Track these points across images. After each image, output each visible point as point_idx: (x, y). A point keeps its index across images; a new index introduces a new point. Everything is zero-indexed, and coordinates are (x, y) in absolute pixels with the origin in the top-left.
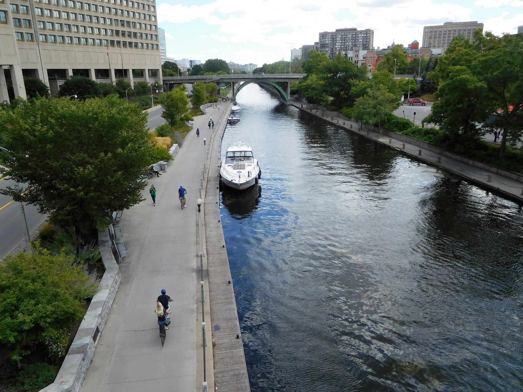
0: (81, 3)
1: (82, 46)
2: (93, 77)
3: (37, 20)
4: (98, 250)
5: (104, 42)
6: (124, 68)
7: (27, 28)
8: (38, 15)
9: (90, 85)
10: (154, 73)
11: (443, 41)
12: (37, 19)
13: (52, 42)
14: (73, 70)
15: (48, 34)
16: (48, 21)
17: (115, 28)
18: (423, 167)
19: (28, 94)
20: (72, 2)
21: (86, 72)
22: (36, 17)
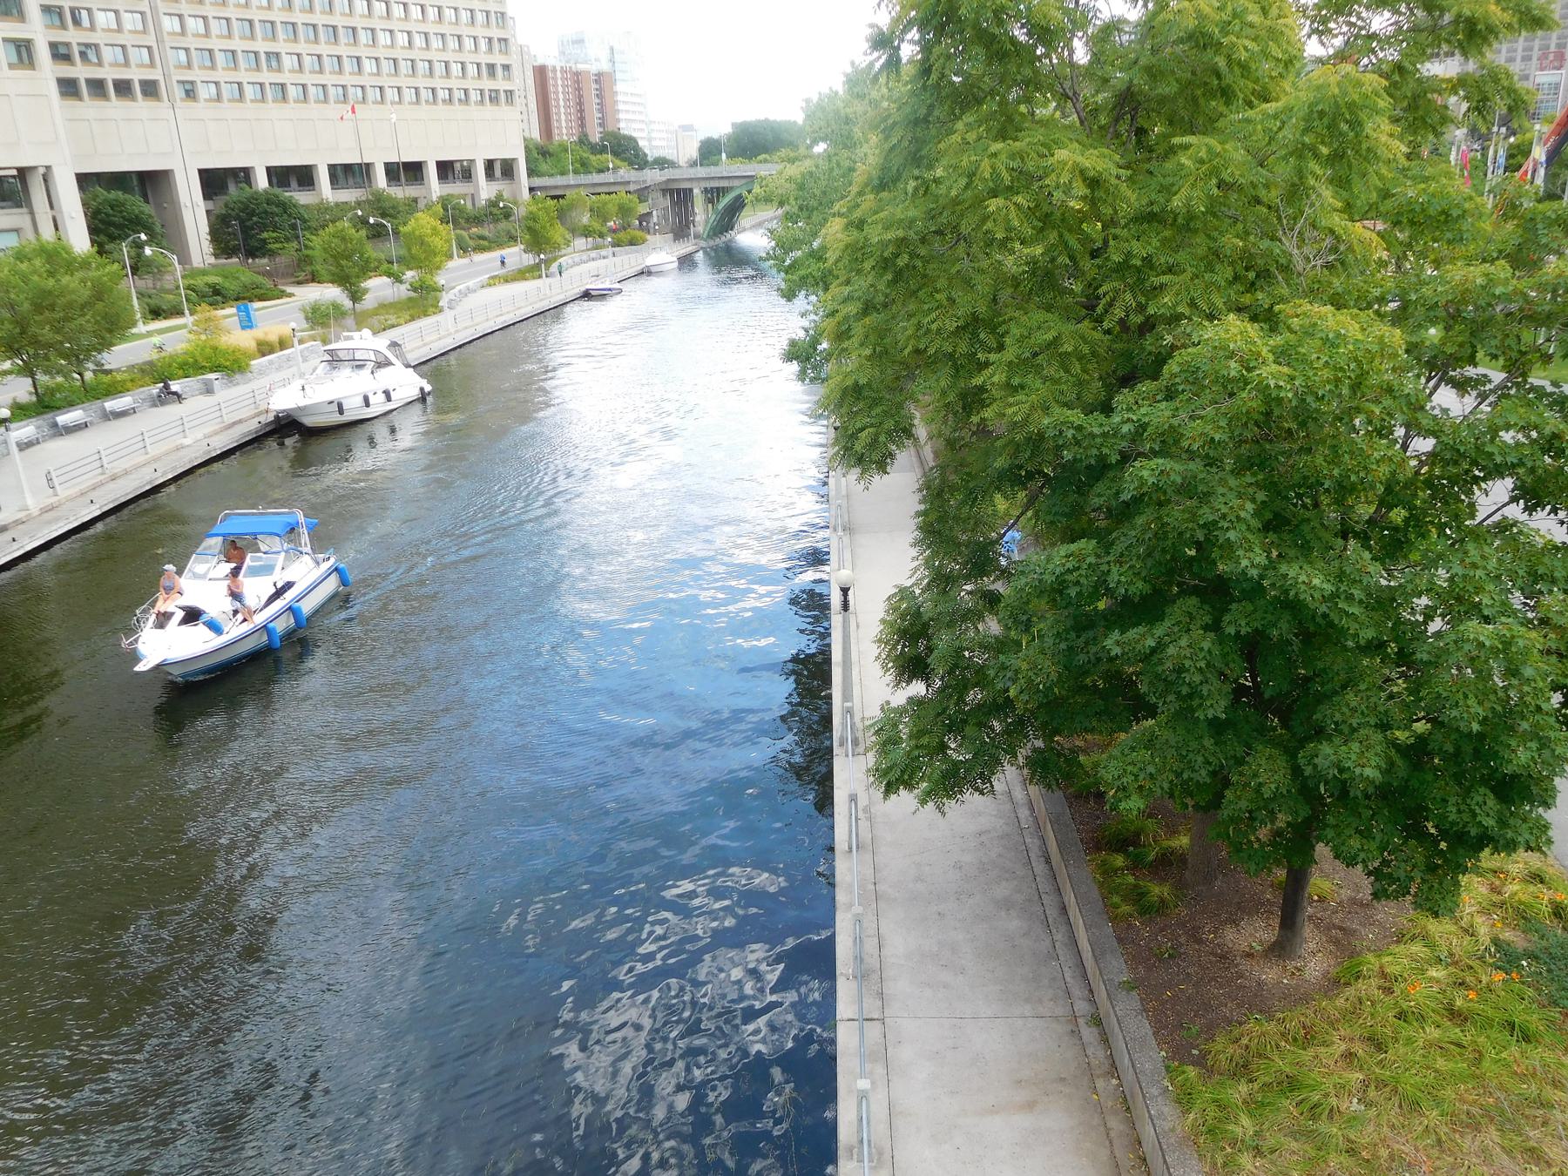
0: (439, 8)
1: (292, 104)
2: (262, 182)
3: (168, 45)
4: (1531, 158)
5: (474, 96)
6: (366, 161)
7: (206, 68)
8: (174, 34)
9: (277, 206)
10: (501, 169)
11: (1508, 51)
12: (169, 42)
13: (210, 100)
14: (201, 172)
15: (367, 84)
16: (173, 45)
17: (485, 59)
18: (1038, 909)
19: (93, 230)
20: (383, 4)
21: (303, 176)
22: (166, 37)
